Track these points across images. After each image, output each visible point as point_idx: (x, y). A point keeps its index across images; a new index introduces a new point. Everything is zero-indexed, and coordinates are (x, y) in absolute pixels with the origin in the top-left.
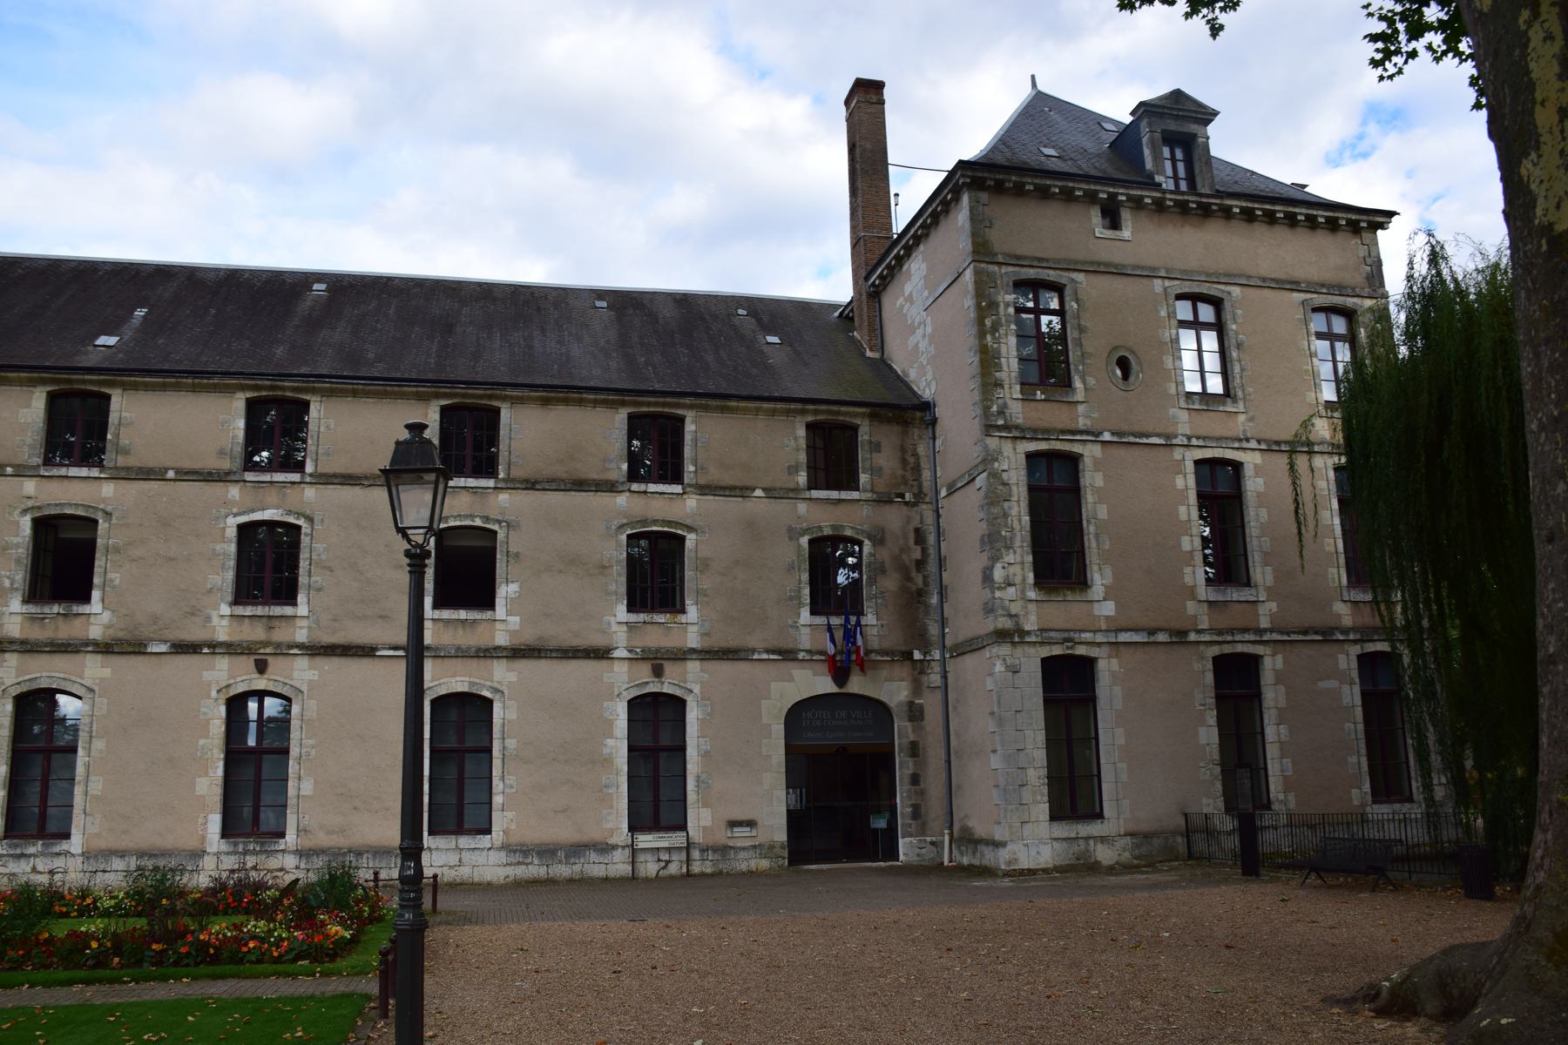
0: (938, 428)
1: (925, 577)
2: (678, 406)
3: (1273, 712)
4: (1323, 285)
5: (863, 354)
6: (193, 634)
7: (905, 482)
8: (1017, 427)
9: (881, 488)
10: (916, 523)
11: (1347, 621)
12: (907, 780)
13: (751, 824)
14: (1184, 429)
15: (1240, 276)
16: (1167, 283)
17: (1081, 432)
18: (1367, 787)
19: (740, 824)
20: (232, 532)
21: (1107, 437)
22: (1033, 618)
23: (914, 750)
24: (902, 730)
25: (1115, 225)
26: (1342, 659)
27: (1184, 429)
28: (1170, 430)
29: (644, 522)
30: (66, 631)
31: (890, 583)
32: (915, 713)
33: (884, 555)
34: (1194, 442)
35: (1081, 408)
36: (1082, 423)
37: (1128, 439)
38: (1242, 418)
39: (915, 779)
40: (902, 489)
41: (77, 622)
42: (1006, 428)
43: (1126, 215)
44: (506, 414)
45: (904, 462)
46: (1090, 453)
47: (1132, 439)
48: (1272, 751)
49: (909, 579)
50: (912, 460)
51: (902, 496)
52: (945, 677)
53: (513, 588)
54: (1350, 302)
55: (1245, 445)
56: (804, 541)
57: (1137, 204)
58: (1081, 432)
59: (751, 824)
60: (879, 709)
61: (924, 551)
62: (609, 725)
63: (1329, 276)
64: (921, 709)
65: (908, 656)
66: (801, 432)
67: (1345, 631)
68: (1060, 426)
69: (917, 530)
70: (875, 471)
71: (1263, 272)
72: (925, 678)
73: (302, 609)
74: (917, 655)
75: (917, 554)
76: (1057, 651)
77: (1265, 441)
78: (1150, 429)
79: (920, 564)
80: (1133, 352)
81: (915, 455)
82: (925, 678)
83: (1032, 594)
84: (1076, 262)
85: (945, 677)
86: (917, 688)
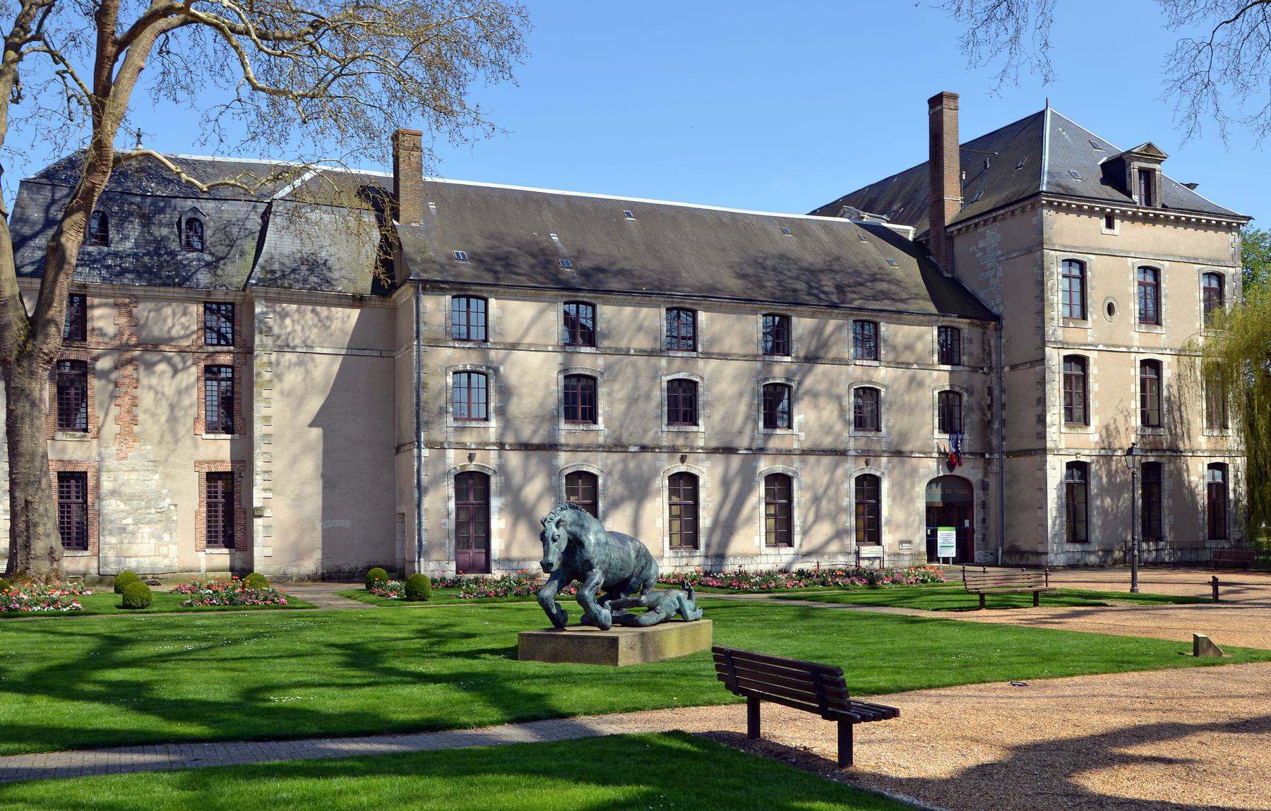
0: (1003, 332)
1: (992, 414)
2: (877, 316)
3: (1167, 492)
4: (1210, 260)
5: (942, 275)
6: (647, 441)
7: (984, 361)
8: (1060, 342)
9: (973, 364)
10: (988, 384)
11: (1204, 446)
12: (980, 520)
13: (910, 542)
14: (1136, 343)
15: (1170, 255)
16: (1134, 260)
17: (1089, 345)
18: (1206, 531)
19: (906, 542)
20: (665, 385)
21: (1101, 347)
22: (1063, 442)
23: (984, 505)
24: (978, 494)
25: (1110, 225)
26: (1200, 466)
27: (1136, 343)
28: (1129, 344)
29: (862, 382)
30: (588, 439)
31: (976, 416)
32: (985, 486)
33: (973, 401)
34: (1141, 350)
35: (1090, 331)
36: (1090, 340)
37: (1111, 349)
38: (1164, 336)
39: (984, 521)
40: (982, 365)
41: (592, 435)
42: (1055, 342)
43: (1117, 222)
44: (794, 319)
45: (984, 350)
46: (1092, 356)
47: (1113, 349)
48: (1165, 512)
49: (984, 415)
50: (987, 349)
51: (982, 369)
52: (1002, 468)
53: (801, 417)
54: (1222, 270)
55: (1164, 352)
56: (936, 393)
57: (1124, 216)
58: (1089, 345)
59: (910, 542)
60: (966, 482)
61: (992, 399)
62: (1172, 527)
63: (1212, 254)
64: (987, 483)
65: (983, 455)
66: (936, 332)
67: (1203, 451)
68: (1079, 342)
69: (989, 388)
70: (971, 354)
71: (1181, 253)
72: (989, 468)
73: (702, 428)
74: (987, 456)
75: (989, 402)
76: (1073, 459)
77: (1175, 349)
78: (1120, 342)
79: (990, 407)
80: (1114, 298)
81: (990, 346)
82: (989, 468)
83: (1063, 430)
84: (1092, 249)
85: (1002, 468)
86: (986, 473)
